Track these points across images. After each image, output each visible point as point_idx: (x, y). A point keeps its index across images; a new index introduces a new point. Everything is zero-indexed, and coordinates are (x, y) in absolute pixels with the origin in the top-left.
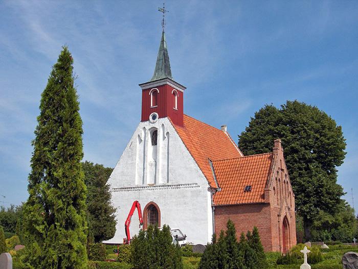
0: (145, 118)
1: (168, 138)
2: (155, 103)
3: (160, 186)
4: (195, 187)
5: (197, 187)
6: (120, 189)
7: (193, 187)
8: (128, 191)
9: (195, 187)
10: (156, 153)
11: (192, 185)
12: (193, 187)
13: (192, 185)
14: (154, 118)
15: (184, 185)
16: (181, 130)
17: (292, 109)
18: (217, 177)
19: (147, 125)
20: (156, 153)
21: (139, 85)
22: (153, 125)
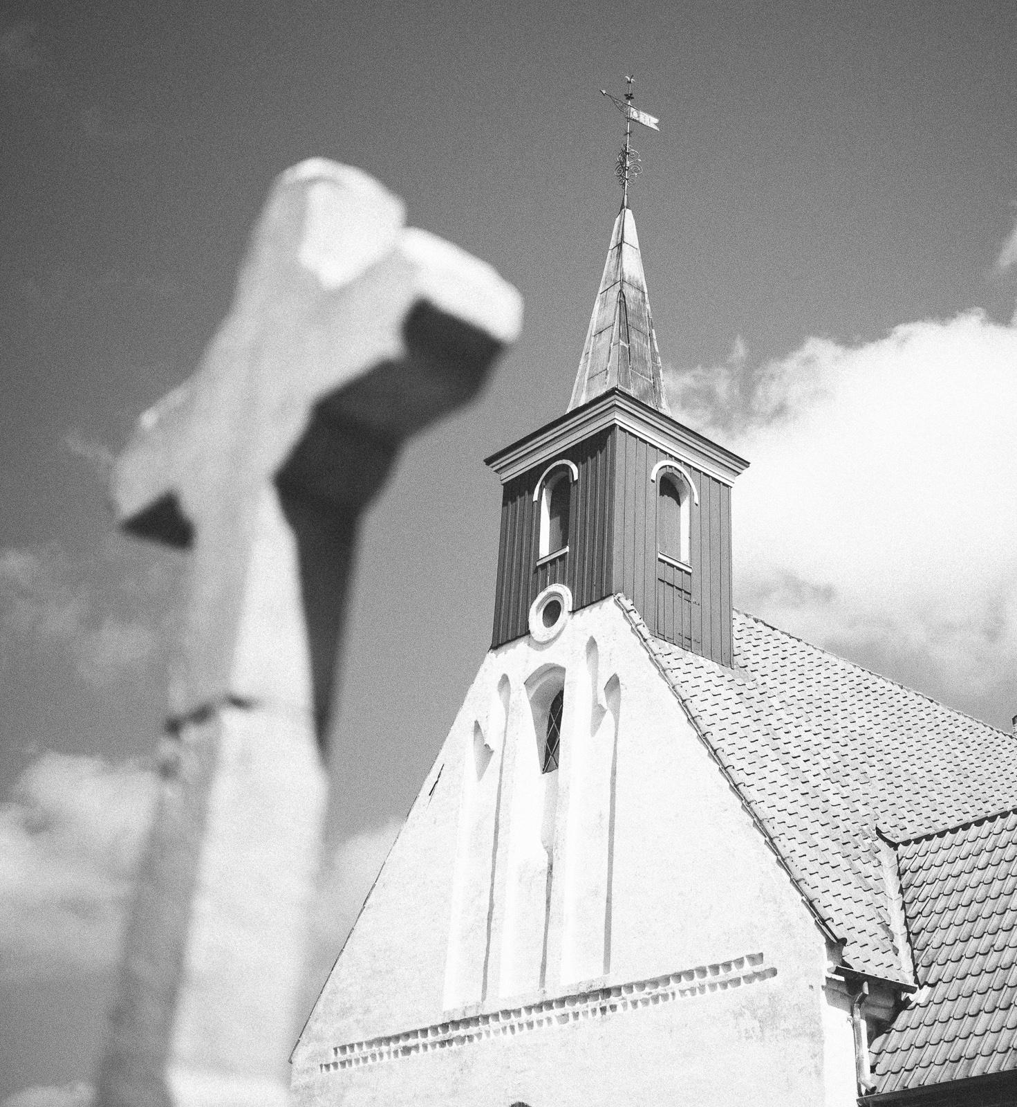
0: (509, 630)
1: (616, 712)
2: (563, 534)
3: (562, 1002)
4: (749, 979)
5: (761, 975)
6: (370, 1044)
7: (737, 982)
8: (407, 1050)
9: (749, 979)
10: (555, 799)
11: (735, 972)
12: (737, 982)
13: (735, 972)
14: (552, 612)
15: (690, 974)
16: (698, 670)
17: (932, 588)
18: (920, 941)
19: (518, 660)
20: (555, 799)
21: (802, 794)
22: (550, 656)
